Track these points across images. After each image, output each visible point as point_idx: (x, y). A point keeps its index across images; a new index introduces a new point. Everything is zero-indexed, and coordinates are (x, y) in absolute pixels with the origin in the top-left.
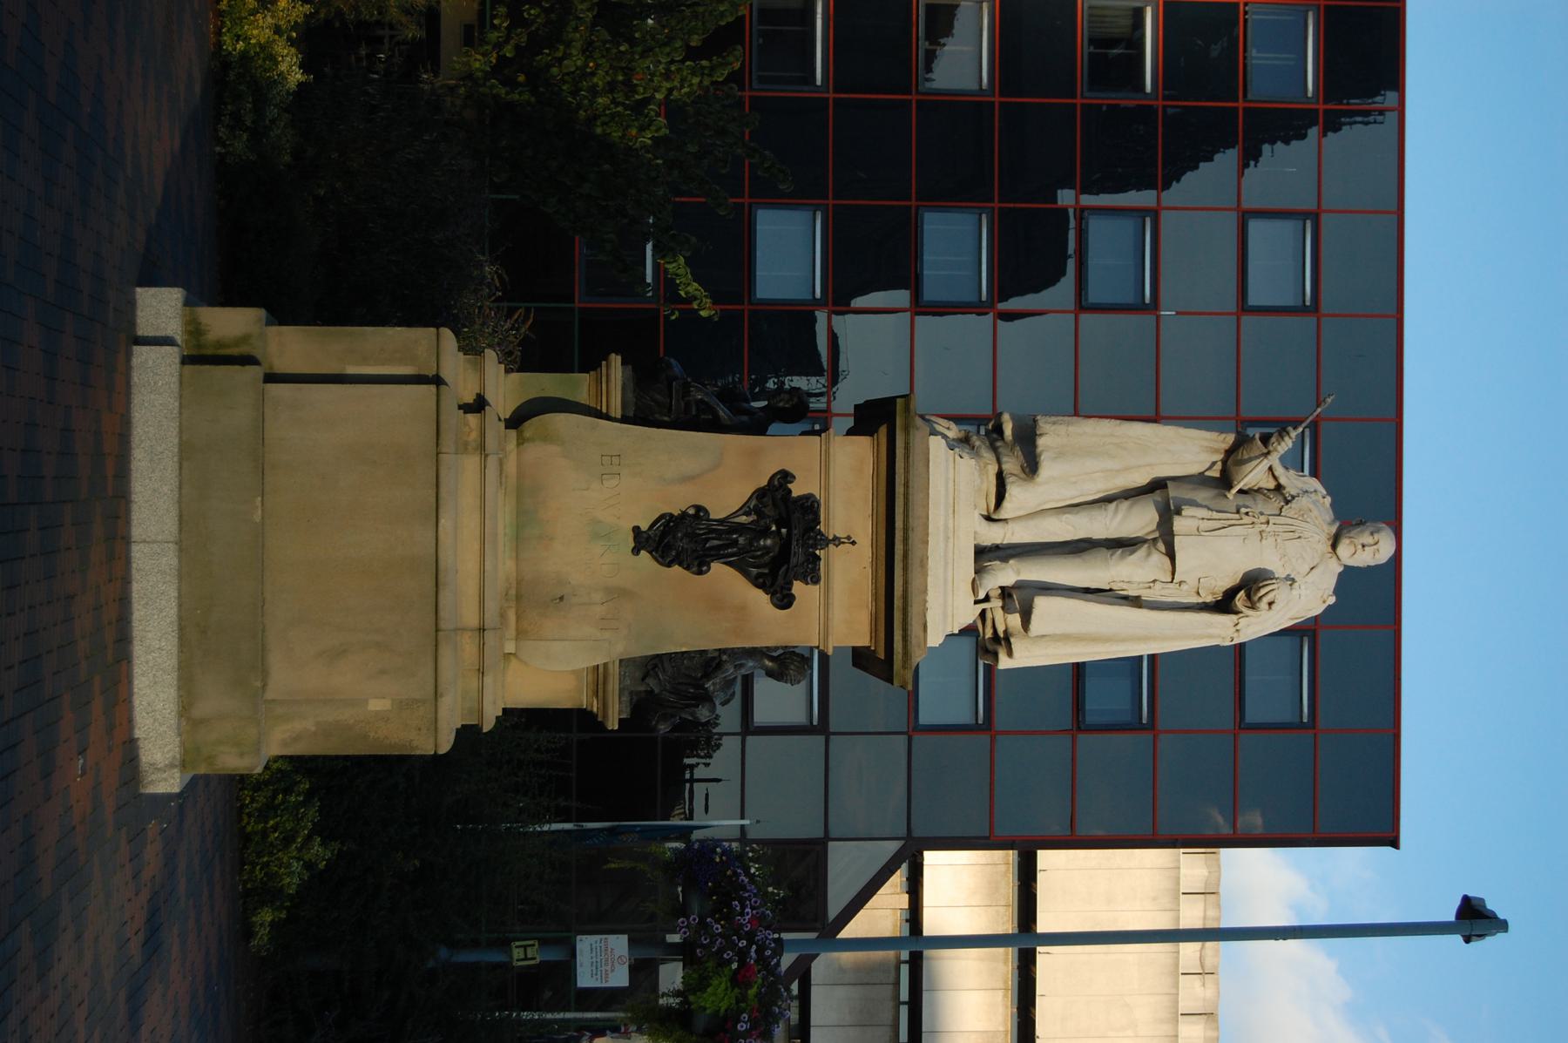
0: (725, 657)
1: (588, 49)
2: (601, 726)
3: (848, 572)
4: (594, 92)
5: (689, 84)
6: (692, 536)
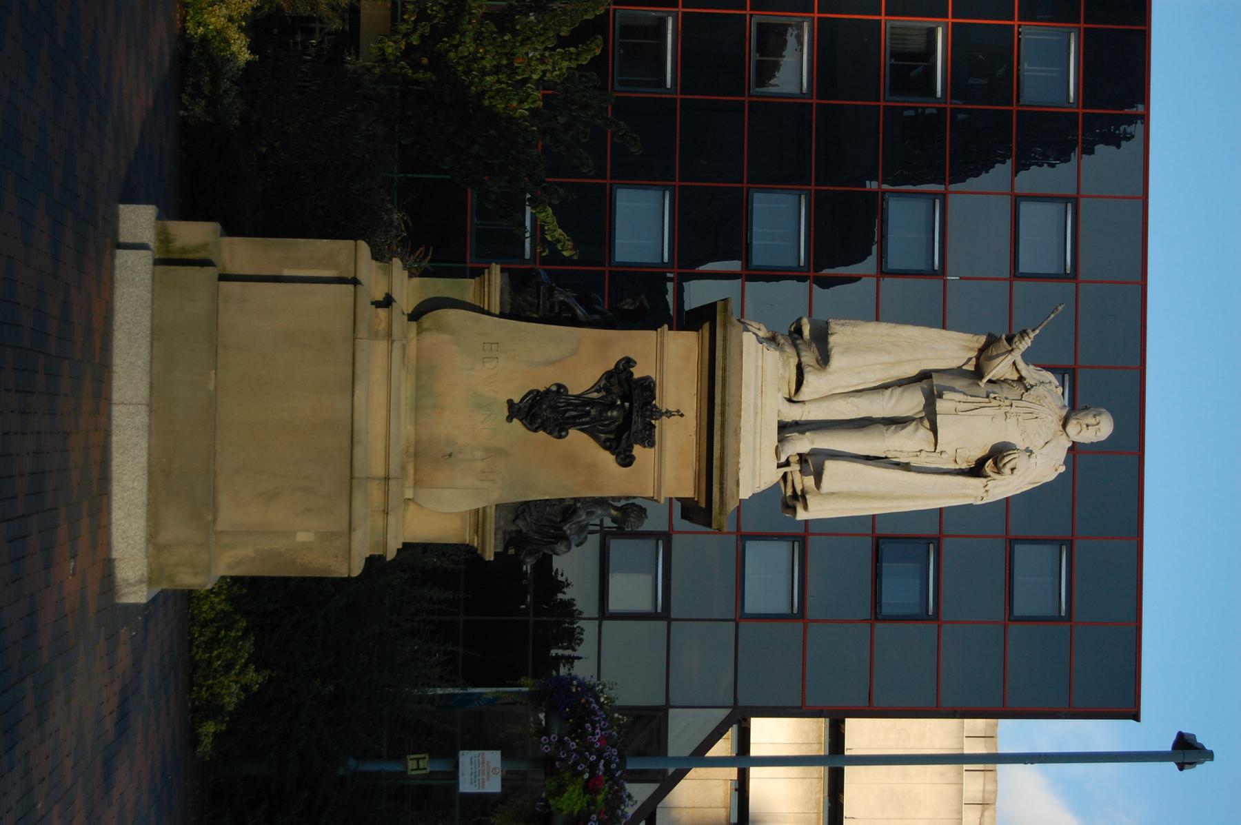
0: (579, 505)
1: (478, 38)
2: (480, 559)
3: (677, 438)
4: (484, 73)
5: (560, 66)
6: (554, 408)
